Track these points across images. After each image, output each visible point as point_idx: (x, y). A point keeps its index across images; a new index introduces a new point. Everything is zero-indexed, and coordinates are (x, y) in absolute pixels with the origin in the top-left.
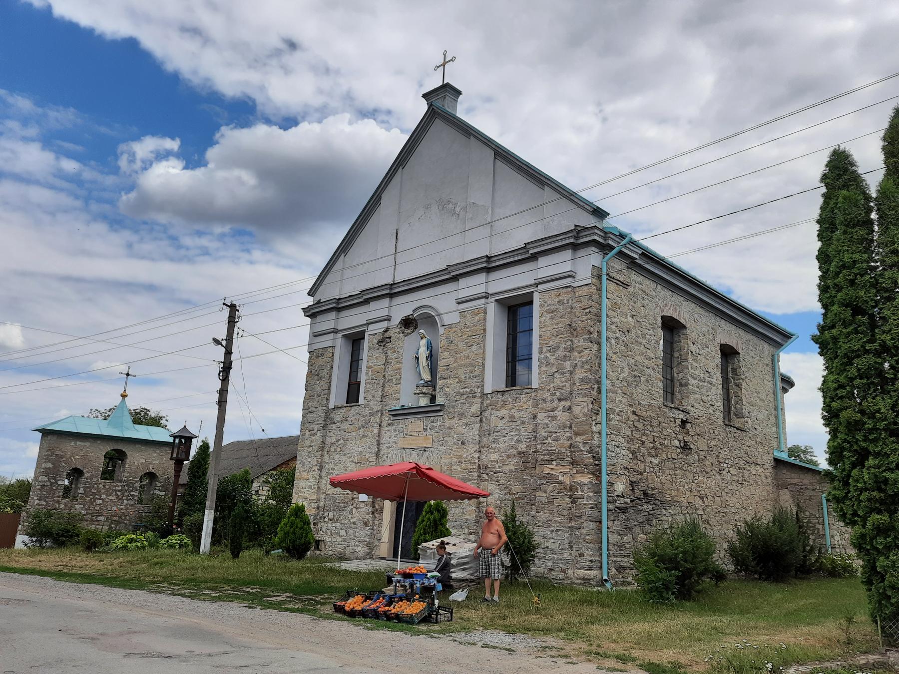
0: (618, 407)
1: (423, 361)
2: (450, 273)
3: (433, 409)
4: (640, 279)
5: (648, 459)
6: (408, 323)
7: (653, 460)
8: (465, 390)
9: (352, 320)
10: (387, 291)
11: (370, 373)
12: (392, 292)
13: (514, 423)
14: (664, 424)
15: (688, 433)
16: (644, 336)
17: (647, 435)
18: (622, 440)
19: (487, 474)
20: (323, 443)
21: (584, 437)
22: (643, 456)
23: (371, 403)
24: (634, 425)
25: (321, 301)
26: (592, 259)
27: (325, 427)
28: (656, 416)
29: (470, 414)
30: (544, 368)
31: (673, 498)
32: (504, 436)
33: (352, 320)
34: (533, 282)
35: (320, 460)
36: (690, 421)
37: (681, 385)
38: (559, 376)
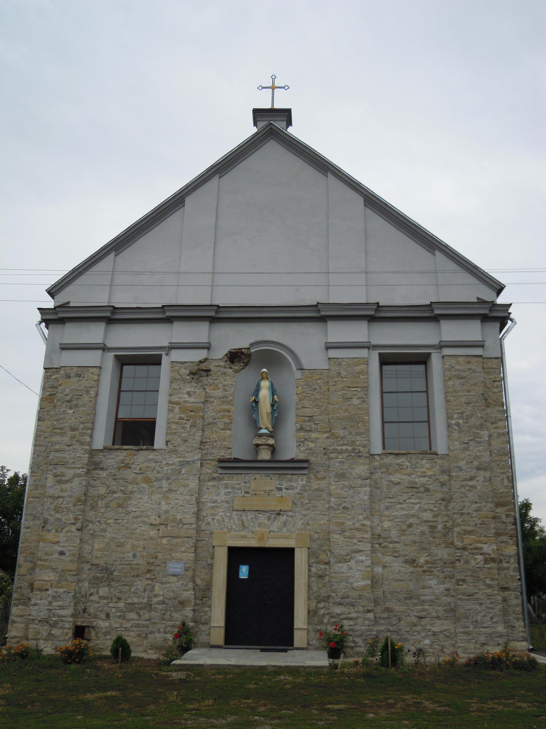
13: (415, 490)
19: (380, 544)
21: (506, 508)
25: (71, 305)
32: (401, 503)
34: (167, 344)
35: (81, 517)
38: (474, 445)
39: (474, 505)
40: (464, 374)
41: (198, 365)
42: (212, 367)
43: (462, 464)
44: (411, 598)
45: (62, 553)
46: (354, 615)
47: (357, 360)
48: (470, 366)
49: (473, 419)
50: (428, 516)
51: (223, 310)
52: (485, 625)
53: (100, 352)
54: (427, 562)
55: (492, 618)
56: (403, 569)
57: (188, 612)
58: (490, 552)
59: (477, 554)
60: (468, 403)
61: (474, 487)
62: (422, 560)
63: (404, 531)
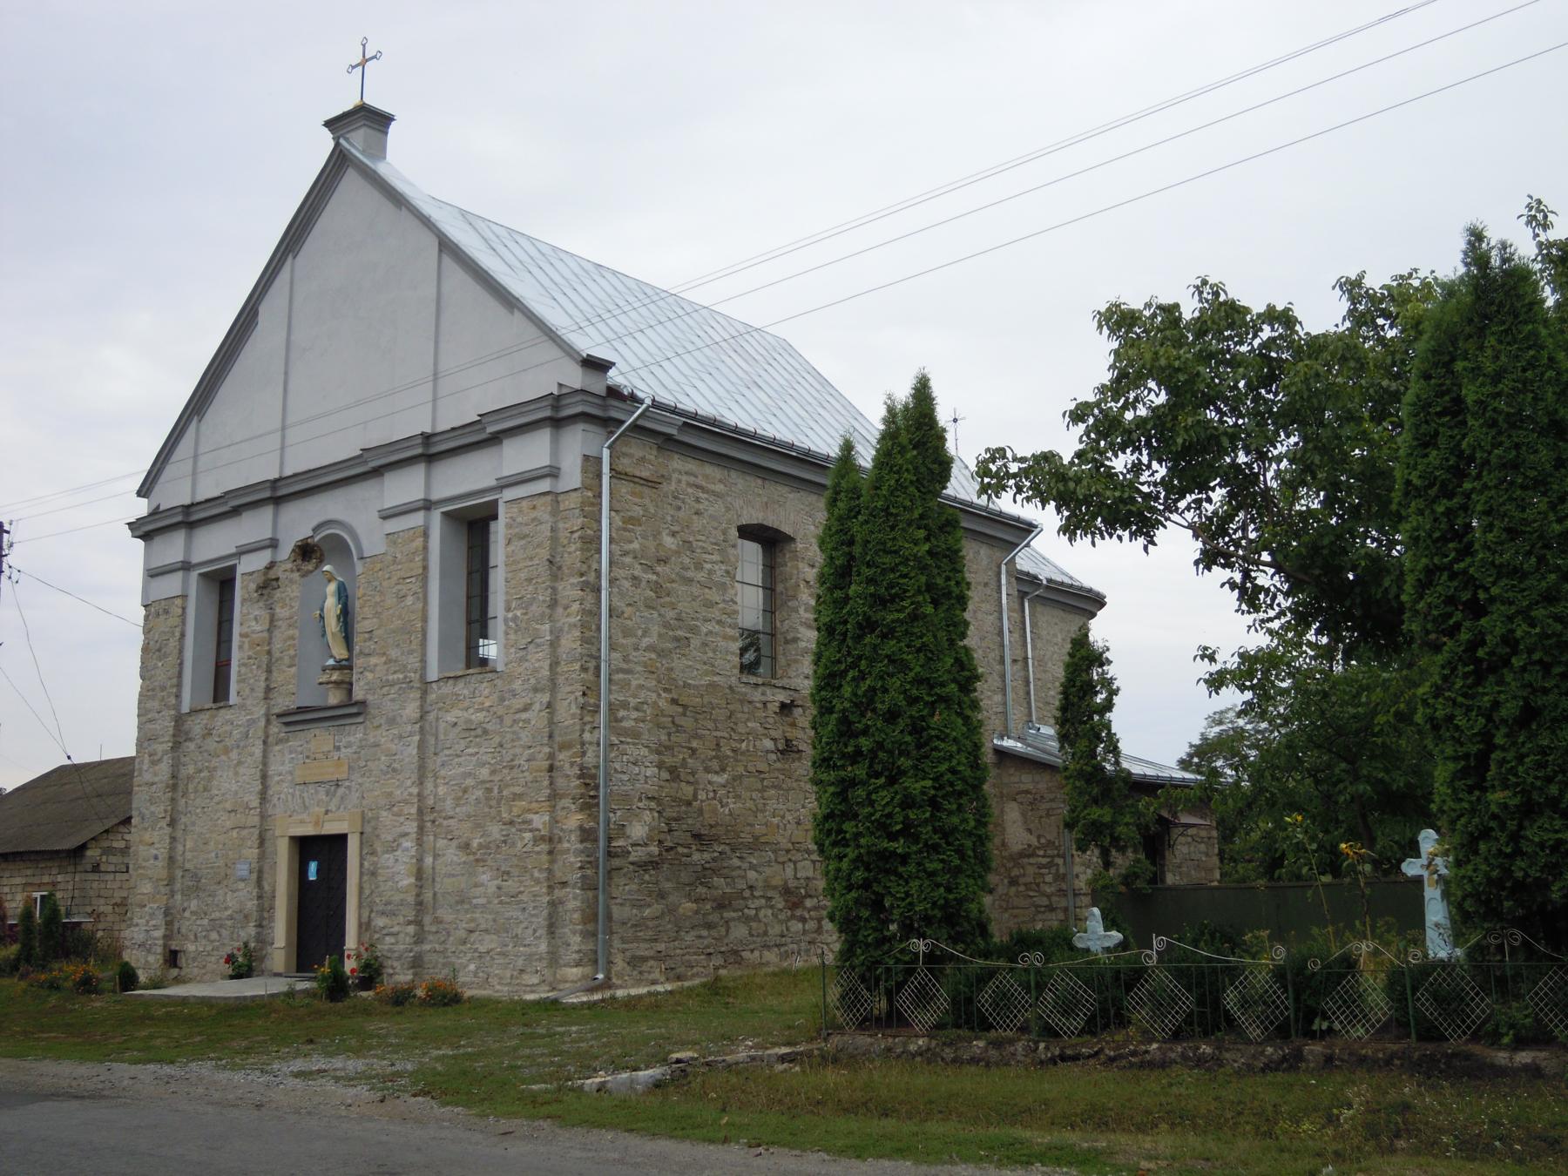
0: (635, 696)
1: (332, 624)
2: (366, 462)
3: (351, 710)
4: (691, 465)
5: (703, 777)
6: (306, 552)
7: (716, 778)
8: (395, 676)
9: (214, 544)
10: (267, 494)
11: (246, 646)
12: (277, 494)
13: (473, 733)
14: (739, 715)
15: (793, 725)
16: (699, 566)
17: (700, 737)
18: (645, 752)
20: (174, 777)
21: (570, 753)
22: (693, 774)
23: (248, 702)
24: (673, 722)
26: (577, 444)
27: (176, 746)
28: (724, 702)
29: (404, 719)
30: (512, 637)
31: (756, 838)
32: (458, 756)
33: (214, 544)
36: (800, 703)
37: (787, 642)
39: (528, 752)
40: (526, 530)
41: (265, 574)
42: (280, 574)
43: (517, 685)
44: (462, 902)
45: (156, 858)
46: (396, 929)
47: (412, 532)
48: (534, 514)
49: (534, 608)
50: (484, 773)
51: (438, 438)
52: (526, 942)
53: (180, 574)
54: (481, 846)
55: (535, 931)
56: (455, 858)
57: (251, 930)
58: (541, 827)
59: (525, 831)
60: (529, 580)
61: (527, 721)
62: (475, 844)
63: (459, 798)
